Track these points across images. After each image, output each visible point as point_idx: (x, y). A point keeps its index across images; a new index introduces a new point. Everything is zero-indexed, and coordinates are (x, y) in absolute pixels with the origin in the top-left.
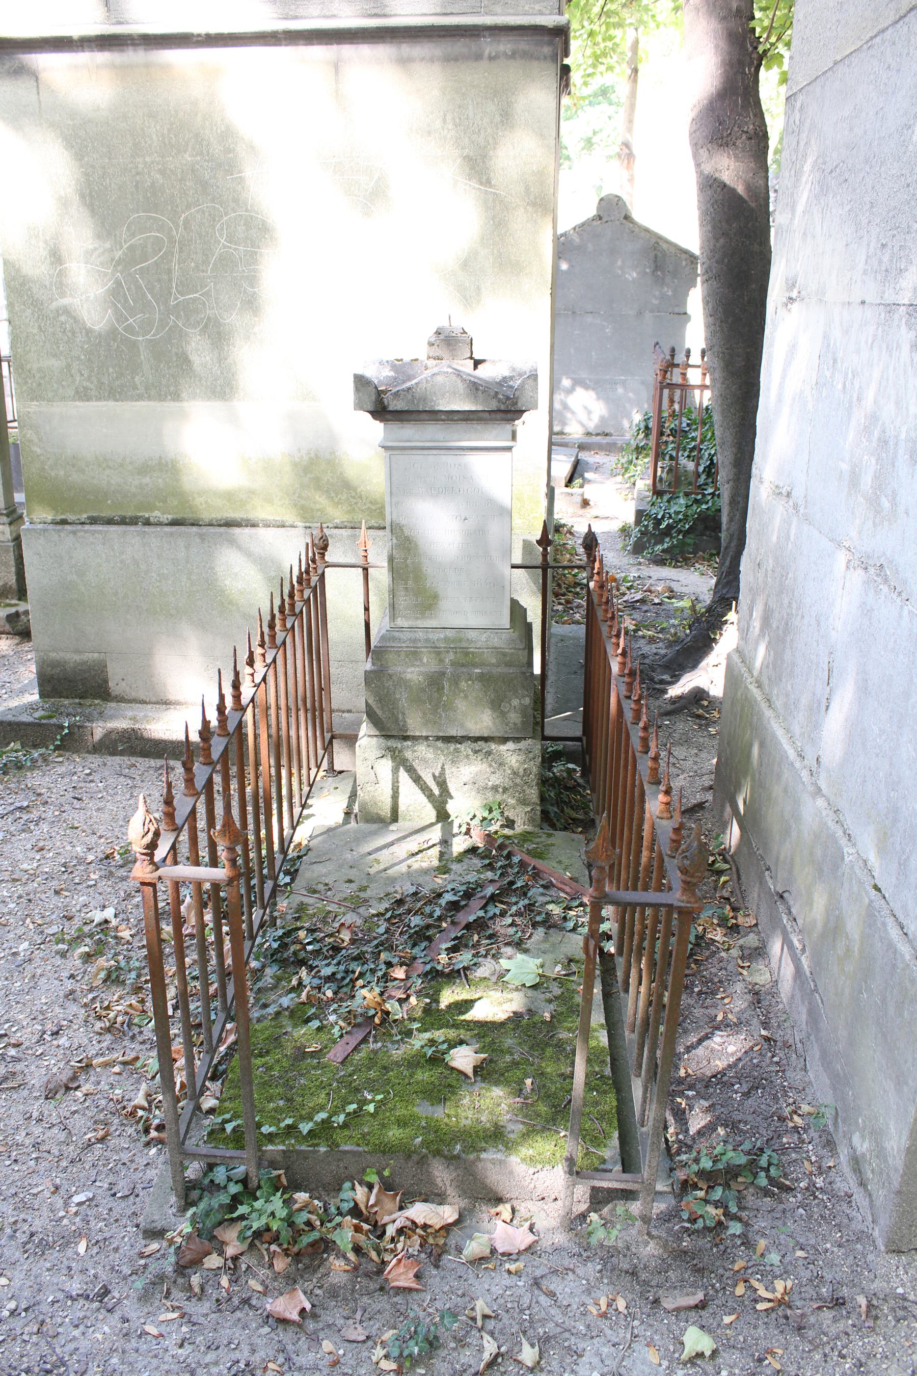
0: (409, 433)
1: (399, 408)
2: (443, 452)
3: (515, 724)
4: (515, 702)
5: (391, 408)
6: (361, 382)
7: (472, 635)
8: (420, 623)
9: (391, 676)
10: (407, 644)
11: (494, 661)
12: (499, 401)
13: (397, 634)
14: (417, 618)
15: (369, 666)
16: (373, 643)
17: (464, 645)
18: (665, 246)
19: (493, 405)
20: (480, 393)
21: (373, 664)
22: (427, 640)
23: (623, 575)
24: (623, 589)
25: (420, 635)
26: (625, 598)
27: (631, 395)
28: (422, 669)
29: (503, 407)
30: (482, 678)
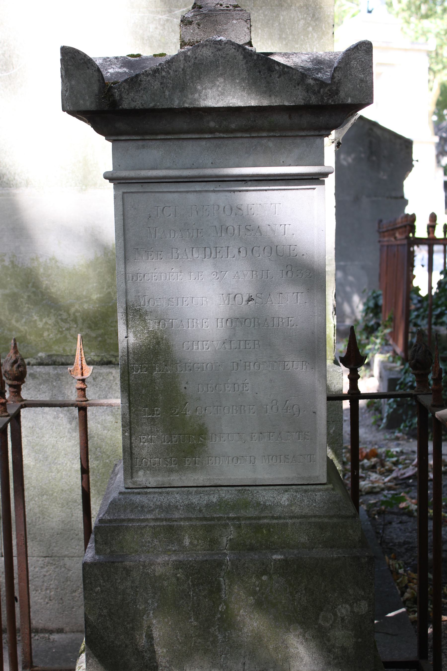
0: (156, 158)
1: (138, 104)
2: (211, 186)
3: (344, 649)
4: (343, 610)
5: (125, 105)
6: (73, 61)
7: (266, 496)
8: (176, 479)
9: (128, 571)
10: (157, 514)
11: (304, 539)
12: (308, 88)
13: (137, 499)
14: (171, 471)
15: (90, 555)
16: (94, 521)
17: (251, 512)
18: (379, 132)
19: (297, 97)
20: (275, 75)
21: (98, 551)
22: (190, 507)
23: (383, 450)
24: (388, 465)
25: (177, 498)
26: (394, 475)
27: (351, 278)
28: (181, 557)
29: (314, 100)
30: (285, 567)
